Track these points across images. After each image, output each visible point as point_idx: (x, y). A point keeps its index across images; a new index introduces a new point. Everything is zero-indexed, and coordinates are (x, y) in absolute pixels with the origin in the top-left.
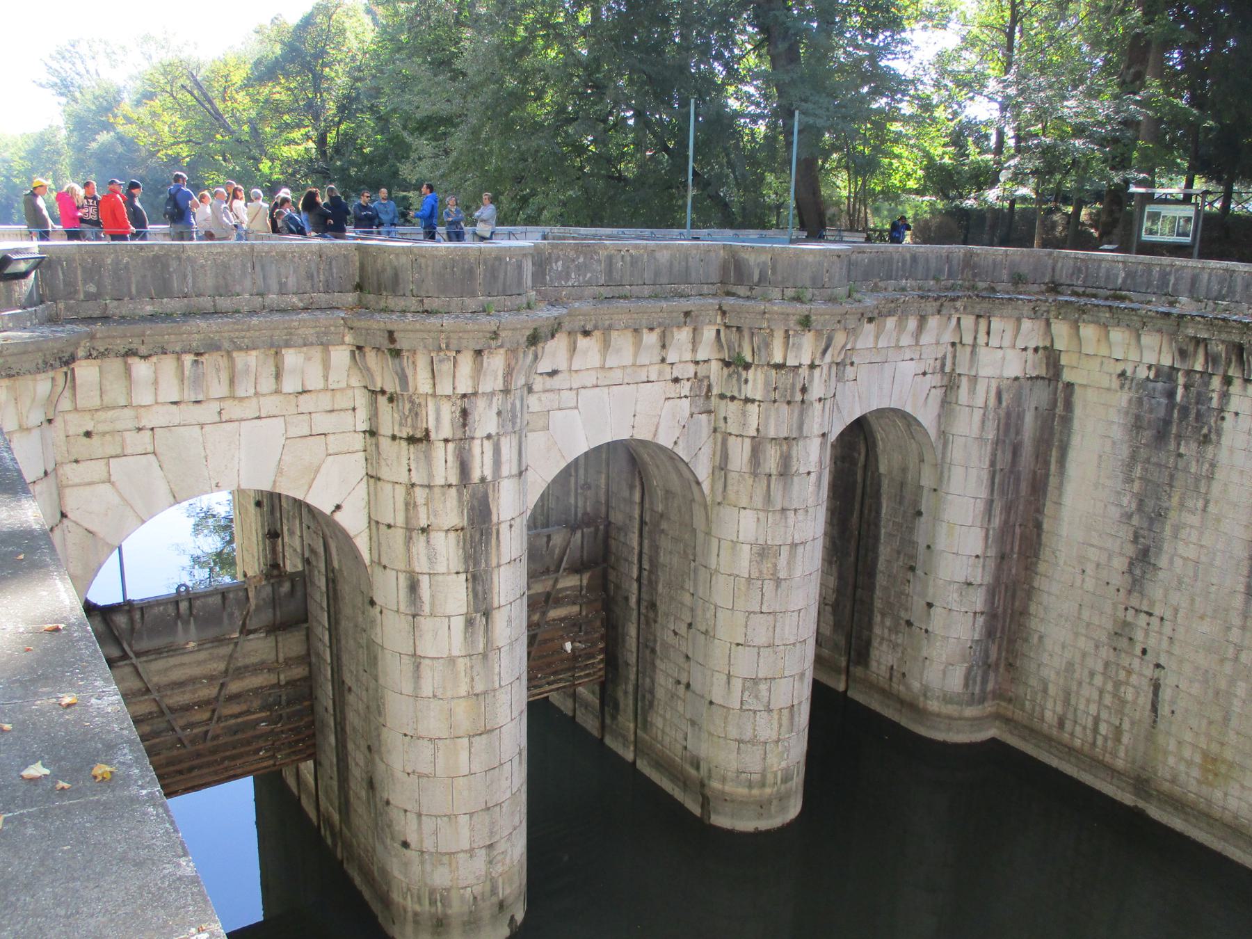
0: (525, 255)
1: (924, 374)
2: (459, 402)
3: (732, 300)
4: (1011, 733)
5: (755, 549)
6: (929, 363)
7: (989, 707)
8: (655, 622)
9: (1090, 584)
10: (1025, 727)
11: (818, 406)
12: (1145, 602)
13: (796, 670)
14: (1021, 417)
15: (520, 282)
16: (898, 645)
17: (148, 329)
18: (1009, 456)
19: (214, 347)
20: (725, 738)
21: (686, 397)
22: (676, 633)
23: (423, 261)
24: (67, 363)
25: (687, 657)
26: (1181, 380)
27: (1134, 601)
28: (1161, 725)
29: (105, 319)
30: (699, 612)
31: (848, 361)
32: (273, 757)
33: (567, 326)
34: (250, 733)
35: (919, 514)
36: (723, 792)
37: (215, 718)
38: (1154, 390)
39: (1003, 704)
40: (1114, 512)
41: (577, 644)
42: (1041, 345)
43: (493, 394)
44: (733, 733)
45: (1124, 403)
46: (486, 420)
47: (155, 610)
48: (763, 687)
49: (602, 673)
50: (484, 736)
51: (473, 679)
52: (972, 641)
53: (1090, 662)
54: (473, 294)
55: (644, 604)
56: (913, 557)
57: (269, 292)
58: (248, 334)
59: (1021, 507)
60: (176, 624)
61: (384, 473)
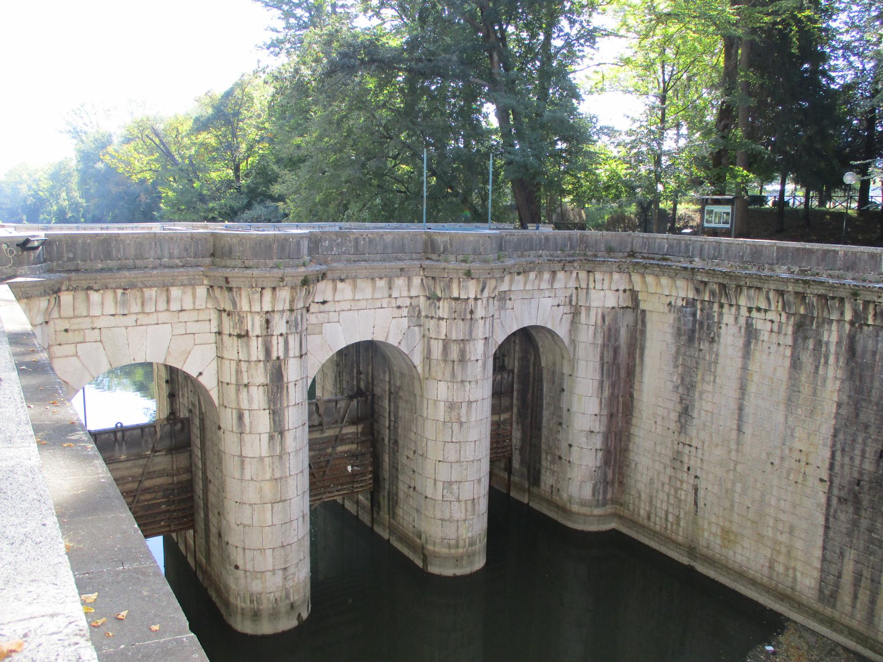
0: (302, 238)
1: (558, 306)
2: (264, 316)
3: (428, 262)
4: (623, 525)
5: (447, 405)
6: (561, 299)
7: (609, 509)
8: (398, 451)
9: (659, 430)
10: (631, 520)
11: (481, 322)
12: (688, 438)
13: (475, 477)
14: (617, 331)
15: (299, 250)
16: (555, 472)
17: (99, 276)
18: (611, 354)
19: (133, 286)
20: (434, 518)
21: (405, 317)
22: (408, 458)
23: (244, 241)
24: (56, 292)
25: (414, 471)
26: (699, 306)
27: (682, 439)
28: (700, 513)
29: (77, 270)
30: (419, 443)
31: (508, 298)
32: (169, 526)
33: (329, 275)
34: (156, 511)
35: (563, 390)
36: (434, 552)
37: (136, 500)
38: (686, 312)
39: (618, 507)
40: (670, 386)
41: (356, 468)
42: (628, 288)
43: (283, 311)
44: (439, 515)
45: (672, 321)
46: (280, 325)
47: (103, 437)
48: (455, 487)
49: (370, 486)
50: (281, 504)
51: (273, 470)
52: (596, 467)
53: (662, 478)
54: (271, 258)
55: (392, 441)
56: (560, 417)
57: (164, 257)
58: (151, 279)
59: (622, 385)
60: (115, 445)
61: (226, 355)
